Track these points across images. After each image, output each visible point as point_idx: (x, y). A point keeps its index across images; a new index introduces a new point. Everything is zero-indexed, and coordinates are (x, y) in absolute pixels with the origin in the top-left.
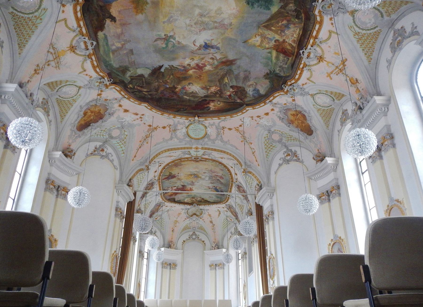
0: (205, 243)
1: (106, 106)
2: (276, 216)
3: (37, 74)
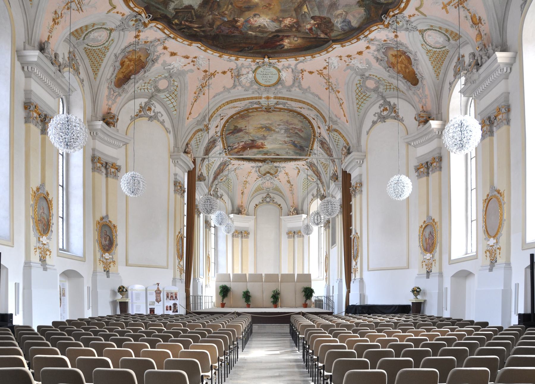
0: (281, 207)
1: (147, 51)
2: (364, 188)
3: (57, 25)
